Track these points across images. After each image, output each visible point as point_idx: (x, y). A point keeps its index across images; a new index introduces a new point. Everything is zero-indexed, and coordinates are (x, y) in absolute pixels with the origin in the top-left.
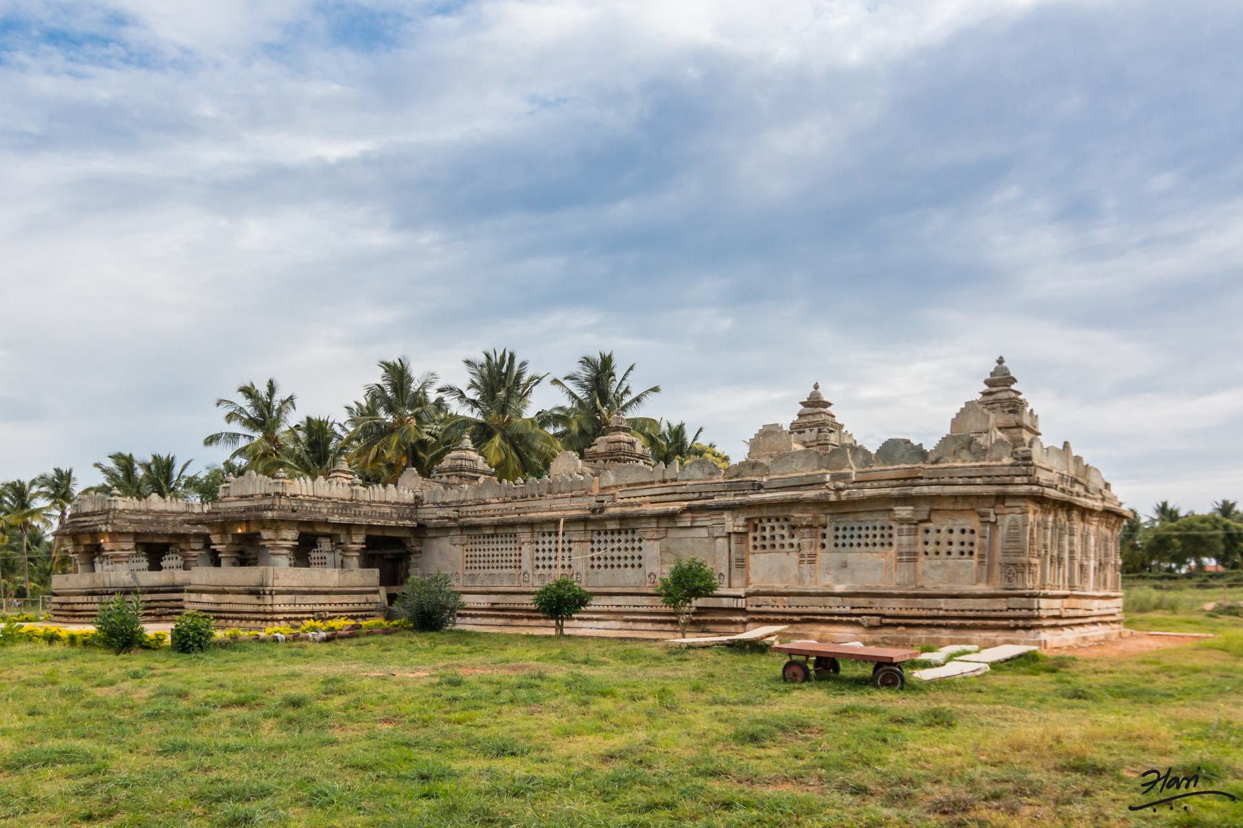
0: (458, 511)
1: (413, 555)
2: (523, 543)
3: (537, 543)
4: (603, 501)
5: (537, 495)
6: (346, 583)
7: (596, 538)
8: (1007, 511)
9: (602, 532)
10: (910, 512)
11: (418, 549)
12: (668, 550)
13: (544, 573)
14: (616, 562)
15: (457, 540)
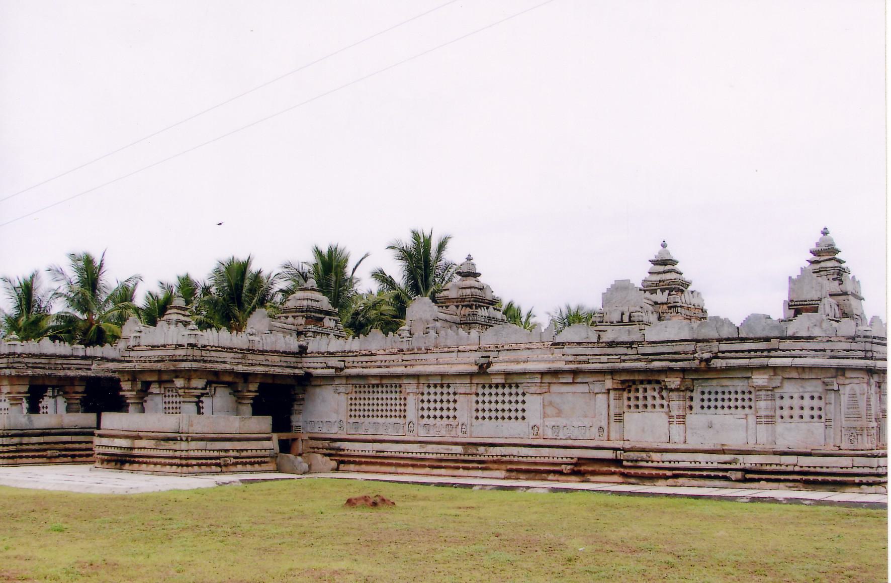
0: (344, 361)
1: (296, 402)
2: (408, 393)
3: (423, 394)
4: (489, 357)
5: (423, 349)
6: (245, 430)
7: (480, 391)
8: (847, 381)
9: (487, 386)
10: (766, 380)
11: (301, 396)
12: (551, 403)
13: (429, 423)
14: (500, 414)
15: (342, 389)
